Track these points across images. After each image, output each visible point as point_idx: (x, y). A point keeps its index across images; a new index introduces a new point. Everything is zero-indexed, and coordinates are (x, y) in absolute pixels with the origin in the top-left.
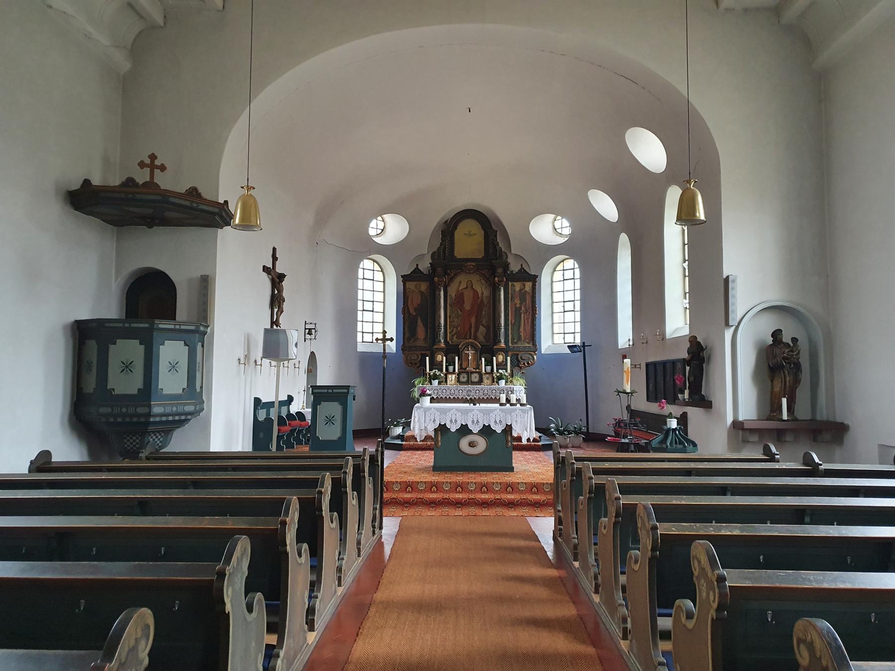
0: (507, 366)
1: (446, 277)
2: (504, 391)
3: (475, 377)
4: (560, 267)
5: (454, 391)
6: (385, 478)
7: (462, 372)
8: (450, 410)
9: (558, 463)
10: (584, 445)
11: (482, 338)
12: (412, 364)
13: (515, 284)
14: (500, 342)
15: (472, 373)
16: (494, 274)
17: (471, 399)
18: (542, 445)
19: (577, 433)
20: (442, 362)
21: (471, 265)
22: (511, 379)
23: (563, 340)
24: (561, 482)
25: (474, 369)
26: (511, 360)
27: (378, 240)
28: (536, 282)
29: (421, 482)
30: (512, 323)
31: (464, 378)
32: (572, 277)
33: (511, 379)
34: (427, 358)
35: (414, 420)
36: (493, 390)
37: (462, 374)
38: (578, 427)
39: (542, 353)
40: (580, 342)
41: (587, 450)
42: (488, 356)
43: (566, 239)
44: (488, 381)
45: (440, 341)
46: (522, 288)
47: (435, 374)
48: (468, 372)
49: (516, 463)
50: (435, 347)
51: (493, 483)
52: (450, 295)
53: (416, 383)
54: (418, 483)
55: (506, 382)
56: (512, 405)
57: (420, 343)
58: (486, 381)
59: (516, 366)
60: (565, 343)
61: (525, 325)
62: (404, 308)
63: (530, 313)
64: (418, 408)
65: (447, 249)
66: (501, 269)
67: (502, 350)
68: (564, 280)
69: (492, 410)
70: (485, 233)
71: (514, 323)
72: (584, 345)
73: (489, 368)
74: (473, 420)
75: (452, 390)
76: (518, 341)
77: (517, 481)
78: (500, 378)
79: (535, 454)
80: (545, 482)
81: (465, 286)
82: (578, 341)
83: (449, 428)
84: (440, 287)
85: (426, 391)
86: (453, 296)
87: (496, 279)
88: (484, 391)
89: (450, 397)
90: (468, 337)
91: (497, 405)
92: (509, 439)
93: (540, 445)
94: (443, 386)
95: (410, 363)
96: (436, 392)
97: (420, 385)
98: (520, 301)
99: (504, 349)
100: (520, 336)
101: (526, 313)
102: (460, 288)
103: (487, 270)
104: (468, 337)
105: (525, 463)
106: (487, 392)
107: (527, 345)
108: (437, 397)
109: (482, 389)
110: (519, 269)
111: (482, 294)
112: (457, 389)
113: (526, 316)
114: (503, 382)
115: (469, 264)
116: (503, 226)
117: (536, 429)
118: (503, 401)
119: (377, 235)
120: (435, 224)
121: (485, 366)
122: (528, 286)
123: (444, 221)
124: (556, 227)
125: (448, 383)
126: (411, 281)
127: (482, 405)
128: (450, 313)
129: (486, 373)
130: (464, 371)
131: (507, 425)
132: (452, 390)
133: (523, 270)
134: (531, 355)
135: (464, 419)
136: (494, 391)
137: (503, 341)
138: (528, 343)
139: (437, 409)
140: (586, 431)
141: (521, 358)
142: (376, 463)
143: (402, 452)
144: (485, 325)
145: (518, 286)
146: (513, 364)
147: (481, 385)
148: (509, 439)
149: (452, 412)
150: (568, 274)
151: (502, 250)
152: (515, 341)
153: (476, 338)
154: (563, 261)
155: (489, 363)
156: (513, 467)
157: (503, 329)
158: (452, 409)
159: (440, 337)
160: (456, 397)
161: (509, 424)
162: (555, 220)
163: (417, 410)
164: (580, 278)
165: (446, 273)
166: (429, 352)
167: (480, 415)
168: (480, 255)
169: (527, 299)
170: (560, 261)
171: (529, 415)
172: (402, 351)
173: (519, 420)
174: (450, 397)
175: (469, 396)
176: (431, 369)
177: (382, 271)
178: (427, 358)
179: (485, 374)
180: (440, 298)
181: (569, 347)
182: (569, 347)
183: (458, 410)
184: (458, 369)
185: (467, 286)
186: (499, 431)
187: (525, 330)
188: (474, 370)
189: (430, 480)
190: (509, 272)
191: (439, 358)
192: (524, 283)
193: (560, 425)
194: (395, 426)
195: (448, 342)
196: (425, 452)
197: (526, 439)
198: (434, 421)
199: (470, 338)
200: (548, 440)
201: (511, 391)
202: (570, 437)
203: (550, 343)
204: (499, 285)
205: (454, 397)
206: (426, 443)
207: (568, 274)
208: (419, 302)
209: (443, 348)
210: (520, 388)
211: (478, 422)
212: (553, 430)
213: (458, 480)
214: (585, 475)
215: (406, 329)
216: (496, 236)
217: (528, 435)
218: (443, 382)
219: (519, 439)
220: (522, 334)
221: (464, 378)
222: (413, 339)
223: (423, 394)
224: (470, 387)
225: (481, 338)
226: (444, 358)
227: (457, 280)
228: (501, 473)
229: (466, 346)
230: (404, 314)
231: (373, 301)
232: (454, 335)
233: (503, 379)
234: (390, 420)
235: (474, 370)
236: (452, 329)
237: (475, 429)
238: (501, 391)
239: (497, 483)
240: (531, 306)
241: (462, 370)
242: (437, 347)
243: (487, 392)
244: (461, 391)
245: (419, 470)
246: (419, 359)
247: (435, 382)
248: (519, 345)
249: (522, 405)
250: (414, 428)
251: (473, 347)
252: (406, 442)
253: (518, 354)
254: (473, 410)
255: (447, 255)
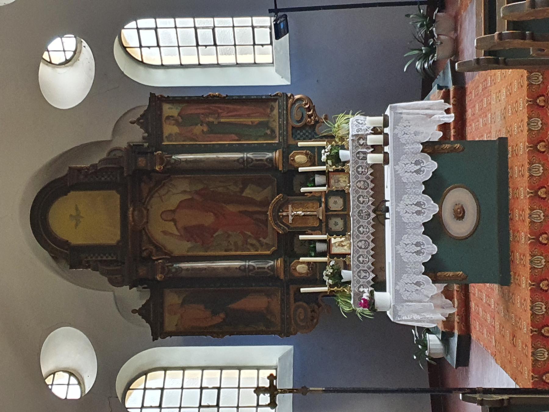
0: (313, 147)
1: (154, 258)
2: (358, 153)
3: (336, 204)
4: (136, 53)
5: (360, 181)
6: (529, 385)
7: (327, 225)
8: (397, 256)
9: (497, 62)
10: (452, 11)
11: (266, 190)
12: (313, 318)
13: (166, 134)
14: (271, 160)
15: (327, 209)
16: (149, 173)
17: (374, 211)
18: (454, 84)
19: (432, 22)
20: (308, 263)
21: (133, 214)
22: (337, 140)
23: (265, 47)
24: (533, 57)
25: (320, 206)
26: (304, 140)
27: (89, 384)
28: (162, 96)
29: (532, 309)
30: (237, 138)
31: (337, 224)
32: (154, 31)
33: (337, 140)
34: (303, 290)
35: (417, 321)
36: (358, 172)
37: (330, 226)
38: (421, 20)
39: (289, 83)
40: (268, 18)
41: (462, 4)
42: (297, 180)
43: (84, 43)
44: (342, 180)
45: (272, 268)
46: (173, 122)
47: (330, 277)
48: (326, 215)
49: (490, 132)
50: (282, 277)
51: (531, 176)
52: (188, 251)
53: (347, 309)
54: (533, 315)
55: (343, 148)
56: (386, 143)
57: (276, 305)
58: (341, 182)
59: (314, 130)
60: (271, 44)
61: (240, 116)
62: (212, 334)
63: (219, 107)
64: (395, 314)
65: (105, 258)
66: (140, 159)
67: (285, 156)
68: (158, 46)
69: (397, 177)
70: (73, 190)
71: (237, 134)
72: (274, 11)
73: (319, 179)
74: (416, 212)
75: (360, 244)
76: (268, 128)
77: (525, 133)
78: (335, 158)
79: (470, 98)
80: (526, 83)
81: (172, 223)
82: (267, 21)
83: (430, 257)
84: (174, 270)
85: (364, 300)
86: (189, 245)
87: (157, 169)
88: (360, 188)
89: (372, 249)
90: (262, 217)
91: (387, 169)
92: (447, 146)
93: (455, 89)
94: (353, 262)
95: (312, 320)
96: (363, 274)
97: (352, 302)
98: (197, 125)
99: (283, 152)
100: (260, 123)
101: (219, 114)
102: (176, 233)
103: (143, 184)
104: (262, 217)
105: (489, 116)
106: (363, 242)
107: (276, 112)
108: (373, 272)
109: (357, 192)
110: (139, 127)
111: (185, 192)
112: (358, 237)
113: (225, 114)
114: (344, 154)
115: (131, 219)
116: (61, 156)
117: (424, 95)
118: (378, 158)
119: (79, 383)
120: (59, 278)
121: (315, 186)
122: (168, 110)
123: (53, 263)
124: (63, 60)
125: (348, 252)
126: (162, 323)
127: (387, 196)
128: (221, 250)
129: (328, 183)
130: (324, 224)
131: (422, 151)
132: (360, 244)
133: (142, 121)
134: (293, 104)
135: (414, 229)
136: (360, 170)
137: (270, 155)
138: (272, 109)
139: (398, 277)
140: (426, 6)
141: (299, 122)
142: (505, 404)
143: (474, 336)
144: (241, 186)
145: (169, 129)
146: (310, 136)
147: (349, 193)
148: (447, 146)
149: (401, 252)
150: (148, 38)
151: (104, 160)
152: (269, 132)
153: (265, 203)
154: (124, 48)
155: (309, 178)
156: (500, 139)
157: (248, 155)
158: (397, 251)
159: (264, 268)
160: (372, 237)
161: (421, 147)
162: (50, 62)
163: (400, 316)
164: (155, 19)
165: (148, 259)
166: (291, 286)
167: (407, 199)
168: (115, 197)
169: (193, 111)
170: (124, 55)
171: (404, 111)
172: (291, 336)
173: (413, 129)
174: (372, 249)
175: (369, 215)
176: (323, 284)
177: (146, 373)
178: (303, 290)
179: (329, 186)
180: (193, 269)
181: (278, 37)
182: (278, 36)
183: (397, 241)
184: (322, 234)
185: (170, 221)
186: (434, 166)
187: (249, 116)
188: (323, 205)
189: (529, 293)
190: (146, 145)
191: (301, 269)
192: (164, 118)
193: (416, 52)
194: (425, 346)
195: (274, 253)
196: (471, 295)
197: (445, 115)
198: (418, 284)
199: (265, 213)
200: (444, 73)
201: (359, 139)
202: (438, 35)
203: (272, 69)
204: (168, 162)
205: (372, 241)
206: (455, 293)
207: (148, 38)
208: (202, 307)
209: (285, 262)
210: (352, 123)
211: (418, 204)
212: (426, 66)
213: (525, 241)
214: (528, 14)
215: (248, 329)
216: (80, 170)
217: (441, 112)
218: (345, 262)
219: (444, 127)
220: (257, 120)
221: (337, 224)
222: (269, 317)
223: (370, 304)
224: (353, 212)
225: (267, 192)
226: (302, 259)
227: (159, 237)
228: (509, 160)
229: (278, 219)
230: (223, 334)
231: (202, 388)
232: (259, 241)
233: (338, 153)
234: (415, 357)
235: (323, 205)
236: (249, 246)
237: (432, 208)
238: (358, 157)
239: (530, 170)
240: (206, 106)
241: (324, 229)
242: (282, 274)
243: (363, 242)
244: (361, 229)
245: (507, 310)
246: (305, 304)
247: (346, 274)
248: (275, 125)
249: (386, 124)
250: (432, 321)
251: (280, 207)
252: (454, 328)
253: (293, 128)
254: (397, 213)
255: (114, 258)
